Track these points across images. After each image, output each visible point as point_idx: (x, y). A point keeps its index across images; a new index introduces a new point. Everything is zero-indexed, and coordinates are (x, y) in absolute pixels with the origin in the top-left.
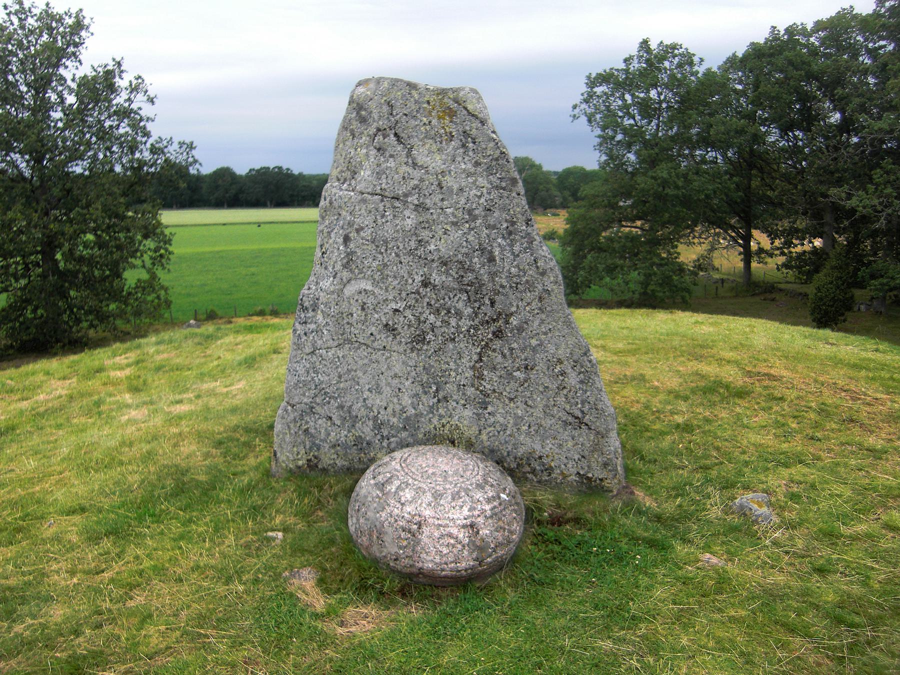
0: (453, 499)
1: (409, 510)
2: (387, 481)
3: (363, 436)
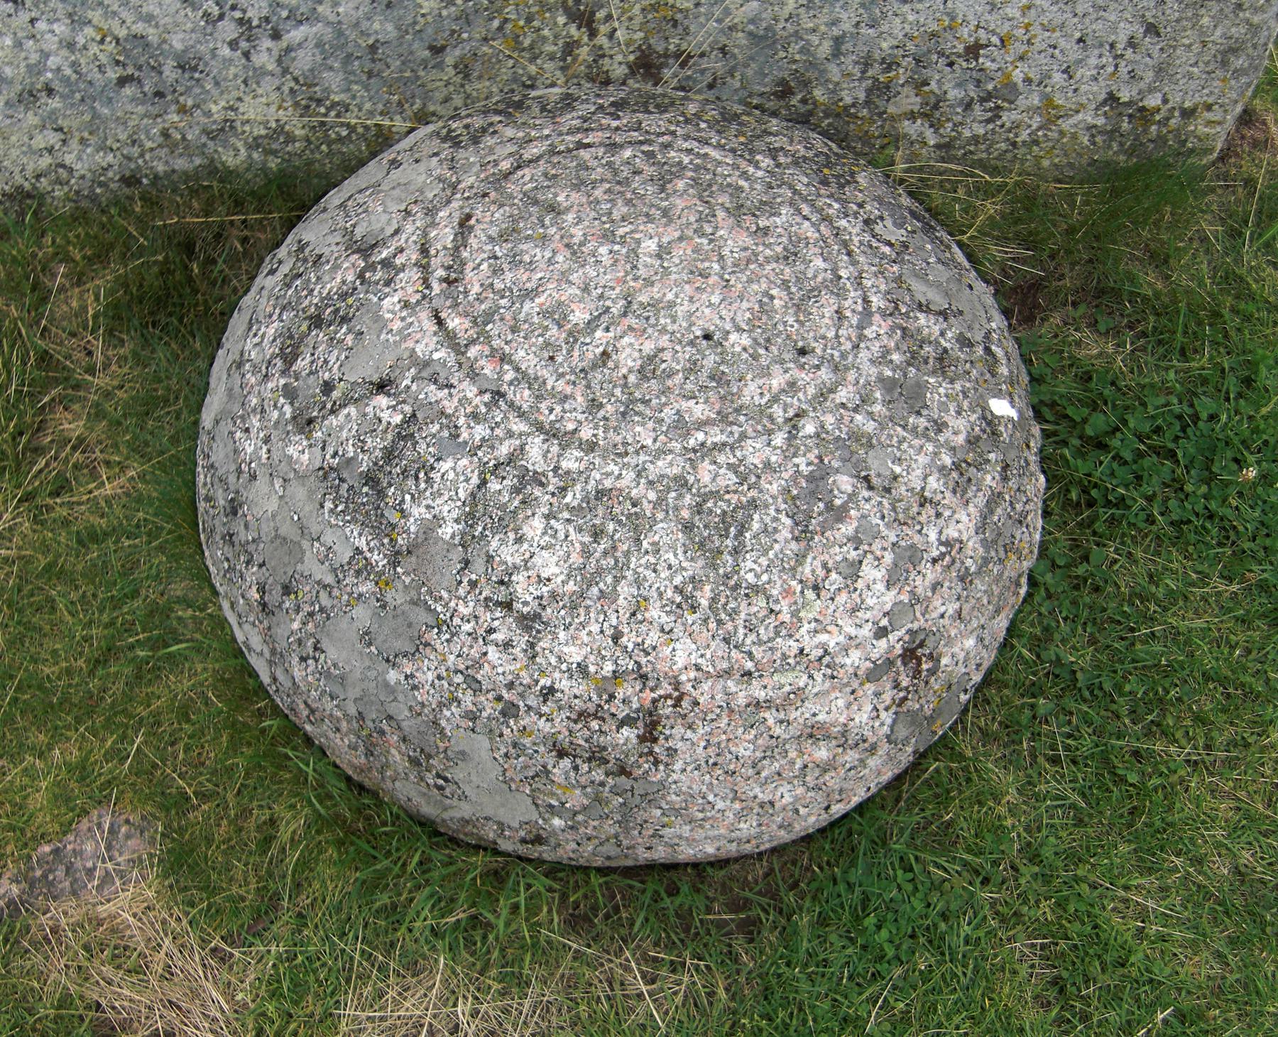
0: (803, 533)
1: (575, 654)
2: (390, 455)
3: (152, 35)
